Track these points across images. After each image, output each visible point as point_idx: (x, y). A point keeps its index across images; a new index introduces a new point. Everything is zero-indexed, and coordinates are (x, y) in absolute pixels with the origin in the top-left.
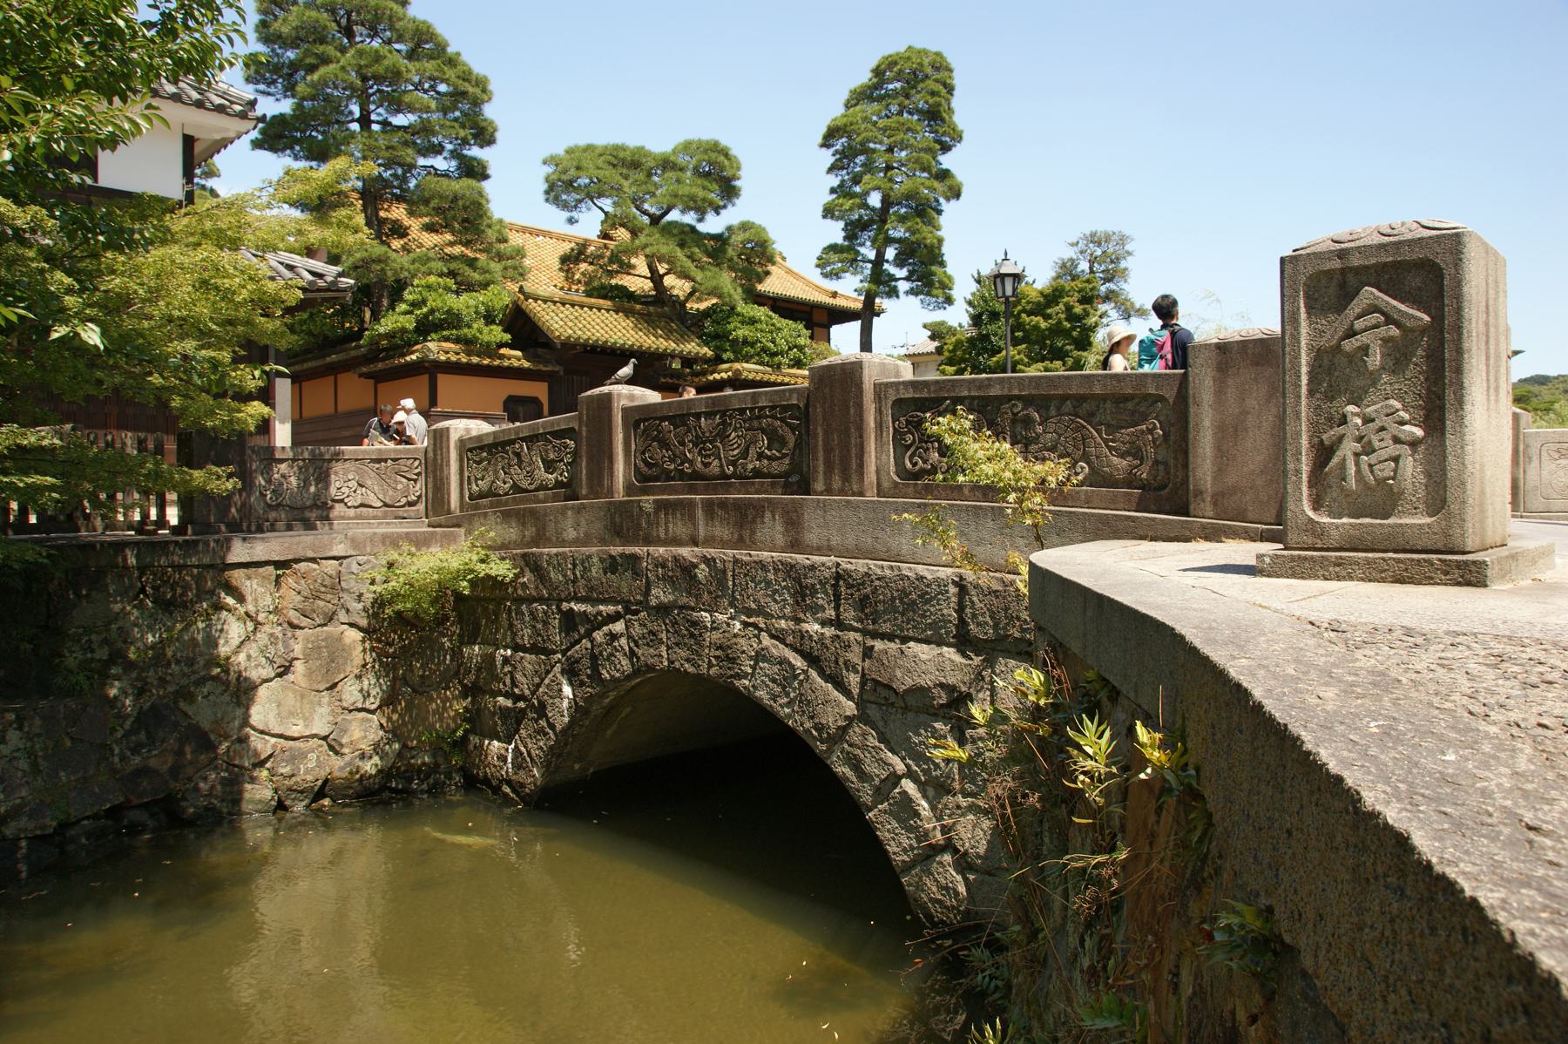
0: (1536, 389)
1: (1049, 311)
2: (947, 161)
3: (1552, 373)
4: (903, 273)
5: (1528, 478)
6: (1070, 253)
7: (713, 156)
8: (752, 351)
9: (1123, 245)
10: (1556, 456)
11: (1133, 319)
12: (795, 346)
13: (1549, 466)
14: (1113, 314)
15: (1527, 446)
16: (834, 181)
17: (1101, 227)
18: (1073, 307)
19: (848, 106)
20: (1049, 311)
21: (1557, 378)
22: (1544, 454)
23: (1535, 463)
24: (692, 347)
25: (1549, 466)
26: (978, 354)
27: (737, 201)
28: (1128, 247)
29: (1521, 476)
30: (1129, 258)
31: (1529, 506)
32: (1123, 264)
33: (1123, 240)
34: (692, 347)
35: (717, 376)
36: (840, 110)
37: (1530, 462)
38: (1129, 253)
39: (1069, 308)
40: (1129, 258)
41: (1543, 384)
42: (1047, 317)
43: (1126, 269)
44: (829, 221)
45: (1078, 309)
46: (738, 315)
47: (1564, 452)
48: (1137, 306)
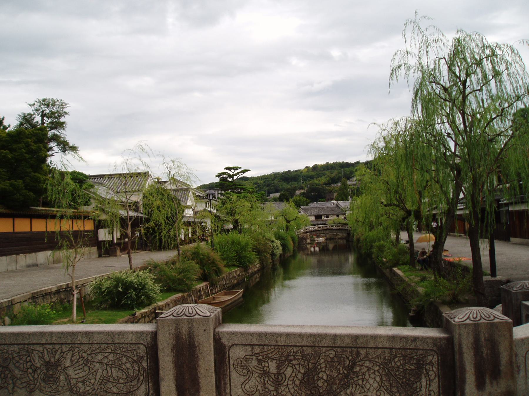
1: (14, 146)
6: (29, 110)
14: (56, 149)
17: (49, 96)
18: (31, 145)
30: (66, 116)
33: (63, 105)
38: (66, 113)
39: (28, 145)
42: (12, 150)
43: (64, 123)
45: (34, 147)
48: (71, 145)
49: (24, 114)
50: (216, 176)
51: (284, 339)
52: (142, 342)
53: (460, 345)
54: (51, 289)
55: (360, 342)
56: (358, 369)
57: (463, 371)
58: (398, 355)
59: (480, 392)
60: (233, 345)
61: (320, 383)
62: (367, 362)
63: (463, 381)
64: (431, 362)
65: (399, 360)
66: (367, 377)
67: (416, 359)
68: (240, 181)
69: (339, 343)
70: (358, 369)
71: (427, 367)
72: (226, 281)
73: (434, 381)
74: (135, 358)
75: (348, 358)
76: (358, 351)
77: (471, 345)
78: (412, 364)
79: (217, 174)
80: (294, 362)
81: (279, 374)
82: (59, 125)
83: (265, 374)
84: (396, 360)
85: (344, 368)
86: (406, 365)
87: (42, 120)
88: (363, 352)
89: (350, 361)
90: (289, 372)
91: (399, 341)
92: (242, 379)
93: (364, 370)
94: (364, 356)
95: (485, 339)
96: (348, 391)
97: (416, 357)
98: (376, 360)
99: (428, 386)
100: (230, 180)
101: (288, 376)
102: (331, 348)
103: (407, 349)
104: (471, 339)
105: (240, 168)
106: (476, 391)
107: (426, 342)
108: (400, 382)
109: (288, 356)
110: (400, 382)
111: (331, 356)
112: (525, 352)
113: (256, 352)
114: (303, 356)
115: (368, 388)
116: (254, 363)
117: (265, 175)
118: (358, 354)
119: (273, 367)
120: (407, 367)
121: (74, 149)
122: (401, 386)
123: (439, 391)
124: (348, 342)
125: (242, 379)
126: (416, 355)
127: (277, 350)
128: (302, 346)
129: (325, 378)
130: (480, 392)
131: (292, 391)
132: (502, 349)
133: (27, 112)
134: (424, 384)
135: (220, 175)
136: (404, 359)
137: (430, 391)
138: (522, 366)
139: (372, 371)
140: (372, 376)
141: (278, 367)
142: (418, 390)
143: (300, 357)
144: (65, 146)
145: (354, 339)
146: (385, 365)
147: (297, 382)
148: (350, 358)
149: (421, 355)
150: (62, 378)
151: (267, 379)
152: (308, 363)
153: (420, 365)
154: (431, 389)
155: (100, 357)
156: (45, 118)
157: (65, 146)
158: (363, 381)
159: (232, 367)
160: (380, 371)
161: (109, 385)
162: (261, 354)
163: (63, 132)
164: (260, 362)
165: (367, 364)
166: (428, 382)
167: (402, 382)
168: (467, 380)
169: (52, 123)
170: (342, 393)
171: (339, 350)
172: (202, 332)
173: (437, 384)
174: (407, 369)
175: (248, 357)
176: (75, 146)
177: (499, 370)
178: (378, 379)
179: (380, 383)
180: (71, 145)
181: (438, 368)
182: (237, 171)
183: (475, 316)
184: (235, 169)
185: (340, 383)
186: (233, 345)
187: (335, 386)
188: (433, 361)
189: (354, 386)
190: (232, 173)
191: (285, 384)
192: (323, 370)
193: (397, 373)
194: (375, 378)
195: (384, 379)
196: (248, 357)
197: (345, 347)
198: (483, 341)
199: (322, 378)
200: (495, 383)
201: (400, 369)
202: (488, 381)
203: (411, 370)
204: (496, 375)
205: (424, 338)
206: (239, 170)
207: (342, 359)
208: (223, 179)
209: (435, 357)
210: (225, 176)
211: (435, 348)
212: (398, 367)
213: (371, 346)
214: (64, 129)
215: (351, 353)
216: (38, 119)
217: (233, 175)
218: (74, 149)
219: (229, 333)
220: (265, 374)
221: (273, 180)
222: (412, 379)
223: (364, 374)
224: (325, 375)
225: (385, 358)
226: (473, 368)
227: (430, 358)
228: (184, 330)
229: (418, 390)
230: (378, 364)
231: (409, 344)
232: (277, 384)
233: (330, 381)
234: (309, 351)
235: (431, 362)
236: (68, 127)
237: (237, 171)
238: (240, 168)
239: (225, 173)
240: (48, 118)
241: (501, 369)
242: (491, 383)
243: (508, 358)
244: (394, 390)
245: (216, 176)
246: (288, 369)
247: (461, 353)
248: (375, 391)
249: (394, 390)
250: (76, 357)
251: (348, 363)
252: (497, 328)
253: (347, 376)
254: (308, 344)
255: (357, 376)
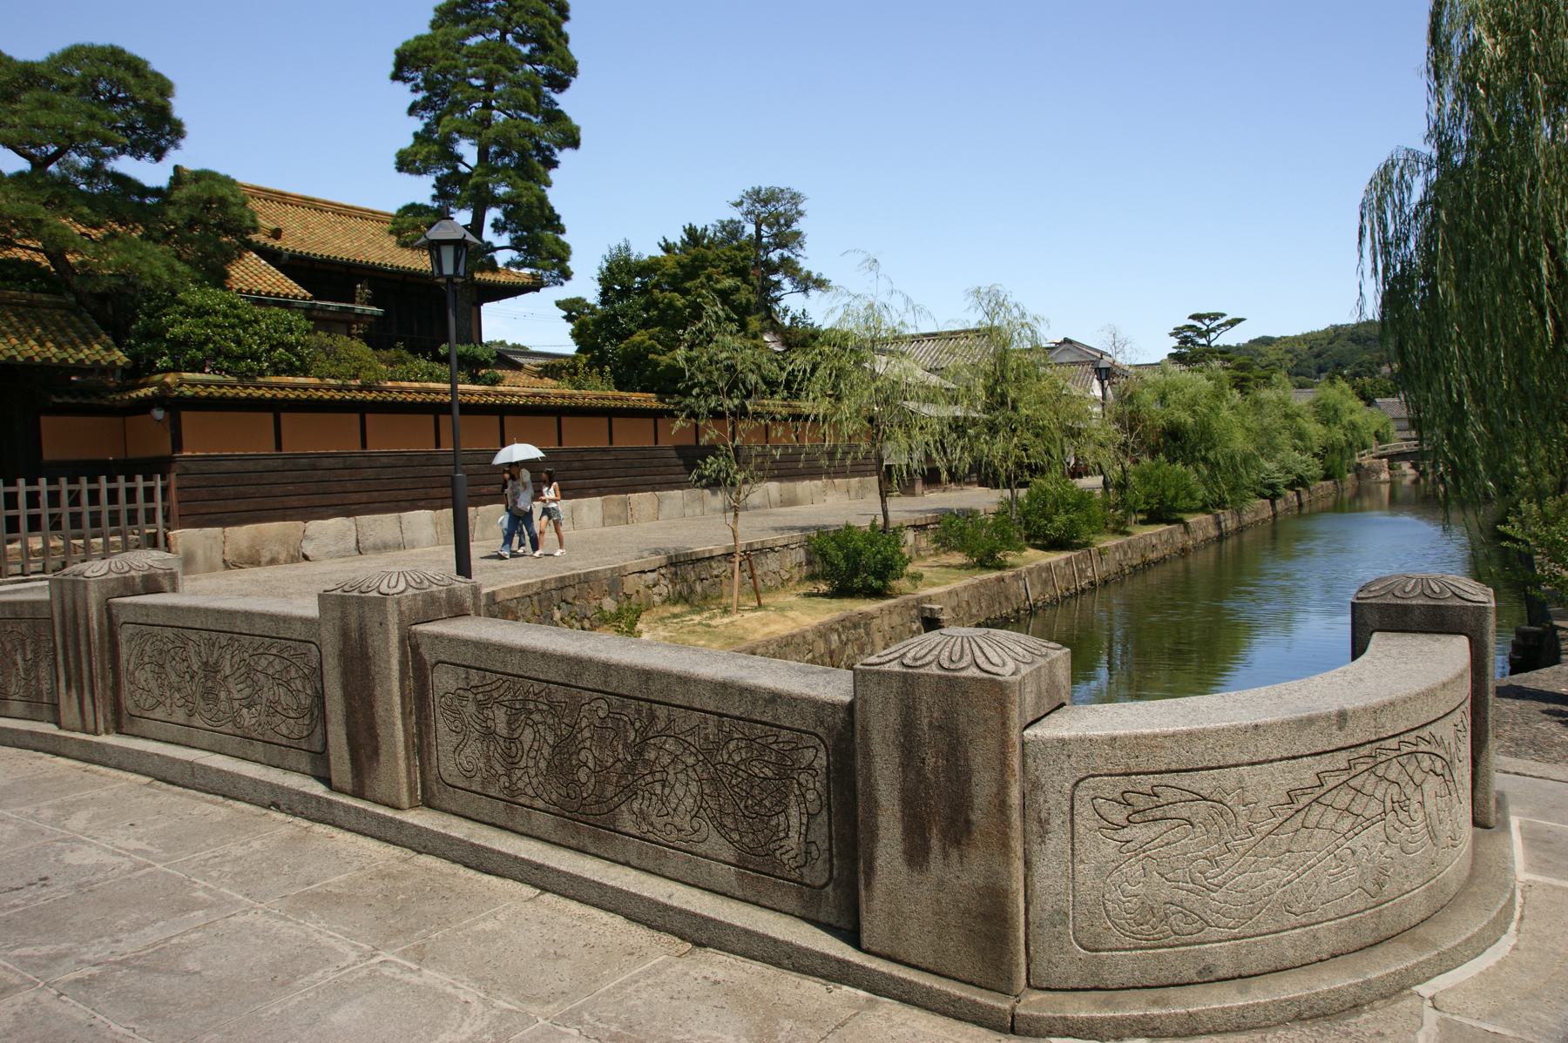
0: (1263, 349)
1: (688, 285)
2: (565, 101)
3: (1276, 335)
4: (505, 239)
5: (1038, 886)
7: (121, 73)
8: (200, 355)
9: (796, 204)
10: (1118, 815)
11: (812, 292)
12: (281, 344)
13: (1099, 849)
14: (787, 284)
15: (1033, 787)
16: (417, 125)
17: (766, 183)
19: (434, 25)
20: (688, 285)
21: (1280, 339)
22: (1084, 811)
23: (1057, 841)
24: (95, 352)
25: (1099, 849)
26: (606, 339)
27: (182, 142)
28: (801, 207)
29: (1018, 885)
31: (1040, 969)
32: (795, 227)
33: (795, 198)
34: (95, 352)
35: (142, 393)
36: (425, 30)
37: (1043, 835)
40: (801, 220)
41: (1268, 344)
44: (405, 176)
46: (181, 303)
47: (1140, 802)
48: (814, 275)
49: (722, 222)
50: (1171, 335)
51: (516, 659)
52: (313, 639)
53: (865, 729)
54: (711, 551)
55: (655, 687)
56: (652, 755)
57: (873, 803)
58: (736, 736)
59: (915, 874)
60: (437, 663)
61: (582, 775)
62: (671, 741)
63: (873, 836)
64: (810, 767)
65: (738, 749)
66: (671, 778)
67: (777, 752)
68: (1256, 347)
69: (614, 684)
70: (652, 755)
71: (803, 778)
72: (1125, 554)
73: (819, 820)
74: (306, 671)
75: (632, 724)
76: (650, 709)
77: (893, 736)
78: (767, 764)
79: (1172, 331)
80: (537, 717)
81: (511, 740)
82: (788, 238)
83: (488, 734)
84: (732, 746)
85: (625, 746)
86: (754, 763)
87: (758, 230)
88: (661, 712)
89: (636, 731)
90: (528, 736)
91: (737, 698)
92: (455, 739)
93: (666, 760)
94: (663, 725)
95: (930, 723)
96: (636, 806)
97: (774, 746)
98: (688, 739)
99: (804, 828)
100: (1203, 341)
101: (526, 748)
102: (600, 695)
103: (757, 722)
104: (893, 718)
105: (1223, 315)
106: (904, 869)
107: (797, 710)
108: (742, 806)
109: (525, 700)
110: (742, 806)
111: (601, 714)
112: (1073, 781)
113: (472, 683)
114: (551, 705)
115: (673, 806)
116: (471, 708)
117: (1312, 333)
118: (653, 717)
119: (500, 718)
120: (757, 771)
121: (820, 284)
122: (744, 816)
123: (830, 849)
124: (631, 685)
125: (455, 739)
126: (775, 742)
127: (507, 684)
128: (548, 682)
129: (591, 765)
130: (915, 874)
131: (535, 781)
132: (979, 760)
133: (726, 219)
134: (794, 821)
135: (1177, 332)
136: (749, 748)
137: (808, 843)
138: (1056, 822)
139: (681, 766)
140: (682, 777)
141: (509, 723)
142: (782, 835)
143: (545, 707)
144: (807, 283)
145: (644, 678)
146: (707, 754)
147: (543, 765)
148: (638, 724)
149: (788, 742)
150: (223, 695)
151: (492, 748)
152: (560, 724)
153: (785, 771)
154: (811, 838)
155: (264, 663)
156: (764, 227)
157: (807, 283)
158: (664, 786)
159: (437, 710)
160: (699, 770)
161: (277, 719)
162: (481, 690)
163: (800, 252)
164: (481, 706)
165: (670, 745)
166: (804, 820)
167: (746, 807)
168: (881, 833)
169: (775, 236)
170: (623, 808)
171: (614, 700)
172: (377, 625)
173: (825, 829)
174: (756, 776)
175: (461, 692)
176: (823, 278)
177: (968, 822)
178: (694, 788)
179: (699, 798)
180: (814, 275)
181: (828, 787)
182: (1218, 322)
183: (393, 583)
184: (1215, 316)
185: (618, 782)
186: (437, 663)
187: (610, 788)
188: (815, 764)
189: (647, 795)
190: (1205, 328)
191: (523, 764)
192: (587, 744)
193: (734, 782)
194: (688, 784)
195: (707, 791)
196: (461, 692)
197: (626, 697)
198: (926, 728)
199: (585, 764)
200: (954, 854)
201: (740, 773)
202: (935, 843)
203: (764, 779)
204: (959, 831)
205: (795, 699)
206: (1222, 321)
207: (621, 723)
208: (1184, 341)
209: (822, 754)
210: (1188, 334)
211: (820, 731)
212: (736, 766)
213: (678, 703)
214: (801, 247)
215: (639, 712)
216: (750, 229)
217: (1209, 331)
218: (820, 284)
219: (438, 637)
220: (488, 734)
221: (1331, 343)
222: (767, 803)
223: (664, 770)
224: (591, 757)
225: (706, 738)
226: (896, 802)
227: (810, 754)
228: (353, 623)
229: (782, 835)
230: (692, 749)
231: (759, 710)
232: (511, 763)
233: (601, 772)
234: (560, 695)
235: (810, 767)
236: (809, 241)
237: (1218, 322)
238: (1223, 315)
239: (1191, 327)
240: (770, 226)
241: (973, 818)
242: (946, 856)
243: (995, 790)
244: (728, 822)
245: (1171, 335)
246: (526, 732)
247: (868, 755)
248: (688, 818)
249: (728, 822)
250: (237, 659)
251: (632, 737)
252: (965, 693)
253: (632, 767)
254: (558, 680)
255: (652, 773)
